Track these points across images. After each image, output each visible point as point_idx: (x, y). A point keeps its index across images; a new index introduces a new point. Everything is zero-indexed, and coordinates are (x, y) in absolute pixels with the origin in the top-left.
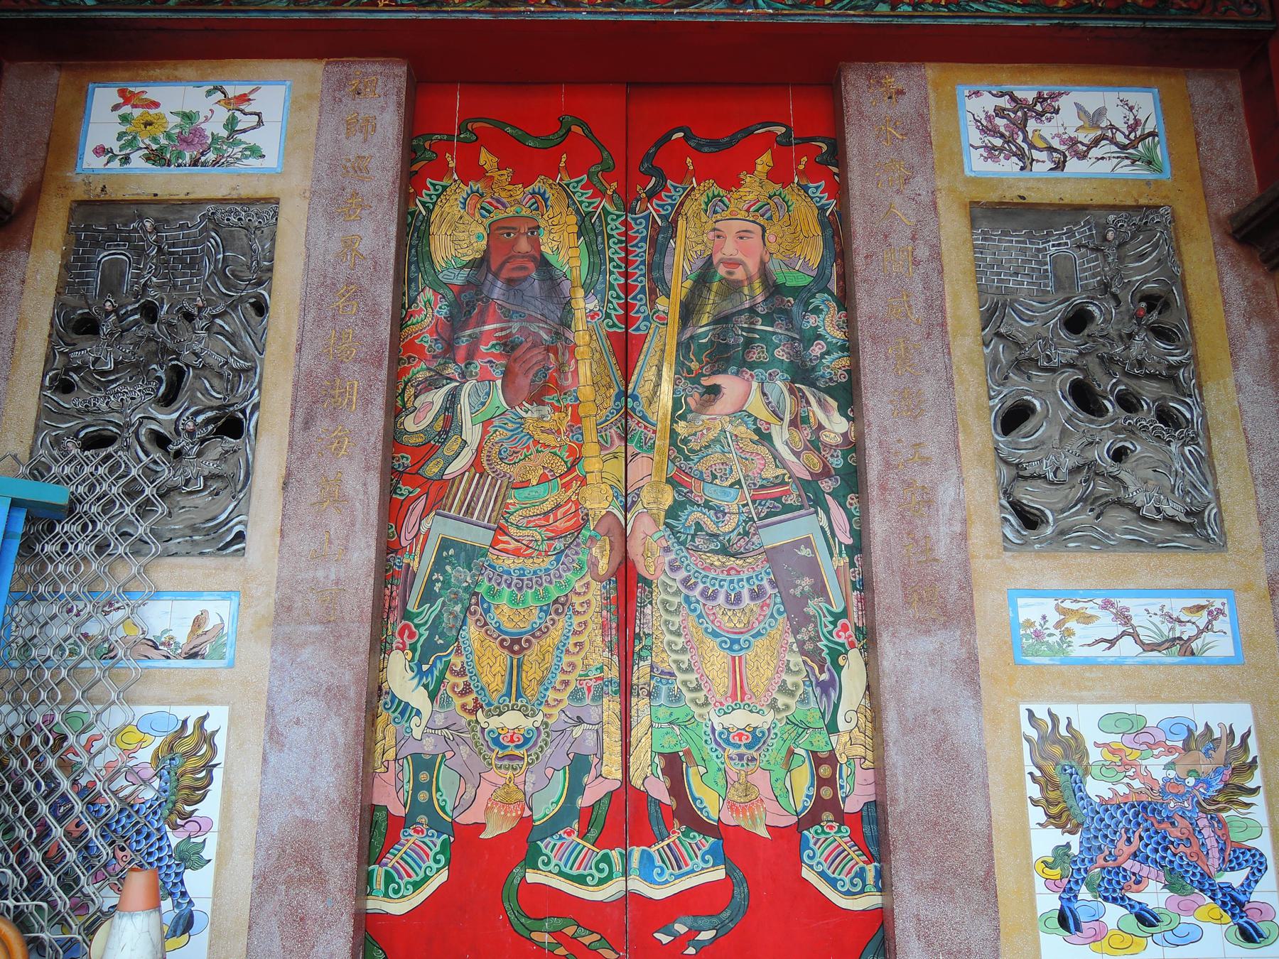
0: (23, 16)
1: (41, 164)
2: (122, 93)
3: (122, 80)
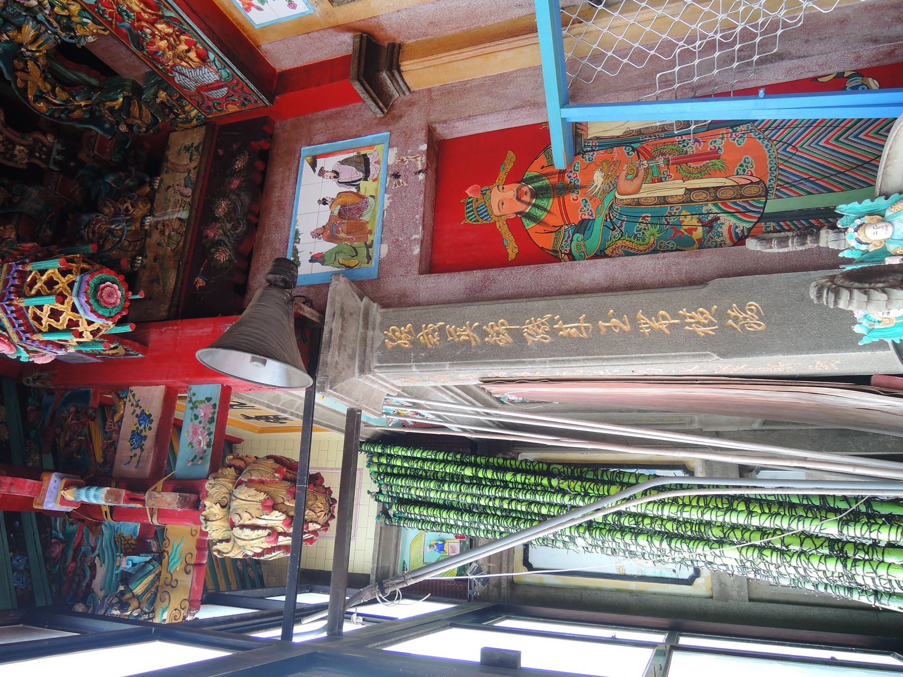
0: (247, 81)
1: (321, 32)
2: (248, 9)
3: (240, 13)
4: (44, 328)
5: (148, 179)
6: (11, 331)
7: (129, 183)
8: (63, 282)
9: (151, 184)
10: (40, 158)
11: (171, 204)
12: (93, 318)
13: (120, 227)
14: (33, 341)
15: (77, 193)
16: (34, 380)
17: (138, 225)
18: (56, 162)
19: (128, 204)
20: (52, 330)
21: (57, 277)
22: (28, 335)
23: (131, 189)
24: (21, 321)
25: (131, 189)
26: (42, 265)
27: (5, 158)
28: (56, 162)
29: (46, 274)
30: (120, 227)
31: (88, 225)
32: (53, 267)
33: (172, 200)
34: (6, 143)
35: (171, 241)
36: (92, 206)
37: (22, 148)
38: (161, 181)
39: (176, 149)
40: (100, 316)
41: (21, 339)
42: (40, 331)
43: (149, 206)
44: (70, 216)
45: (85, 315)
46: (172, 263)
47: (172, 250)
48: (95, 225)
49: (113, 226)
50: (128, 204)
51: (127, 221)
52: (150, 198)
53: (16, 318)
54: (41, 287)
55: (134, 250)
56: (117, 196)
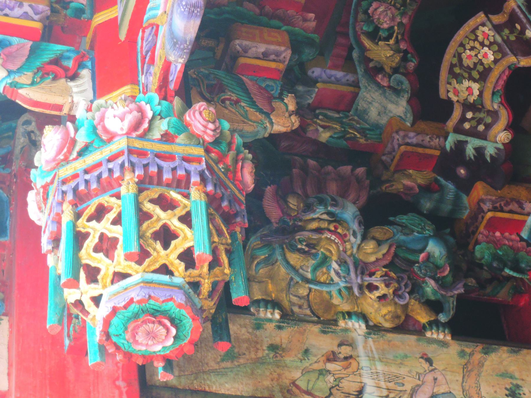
4: (83, 225)
5: (443, 318)
6: (79, 166)
7: (430, 287)
8: (171, 256)
9: (435, 324)
10: (463, 119)
11: (394, 369)
12: (105, 309)
13: (336, 279)
14: (61, 204)
15: (407, 182)
16: (29, 134)
17: (346, 307)
18: (460, 146)
19: (383, 290)
20: (80, 238)
21: (178, 246)
22: (70, 197)
23: (415, 289)
24: (94, 186)
25: (415, 289)
26: (200, 219)
27: (452, 66)
28: (460, 146)
29: (184, 227)
30: (336, 279)
31: (335, 219)
32: (196, 237)
33: (403, 371)
34: (480, 68)
35: (313, 377)
36: (378, 213)
37: (476, 93)
38: (444, 344)
39: (513, 369)
40: (107, 322)
41: (64, 182)
42: (78, 215)
43: (387, 325)
44: (361, 170)
45: (111, 294)
46: (267, 383)
47: (294, 383)
48: (334, 232)
49: (335, 265)
50: (383, 290)
51: (349, 289)
52: (405, 326)
53: (99, 177)
54: (159, 219)
55: (293, 304)
56: (402, 268)
